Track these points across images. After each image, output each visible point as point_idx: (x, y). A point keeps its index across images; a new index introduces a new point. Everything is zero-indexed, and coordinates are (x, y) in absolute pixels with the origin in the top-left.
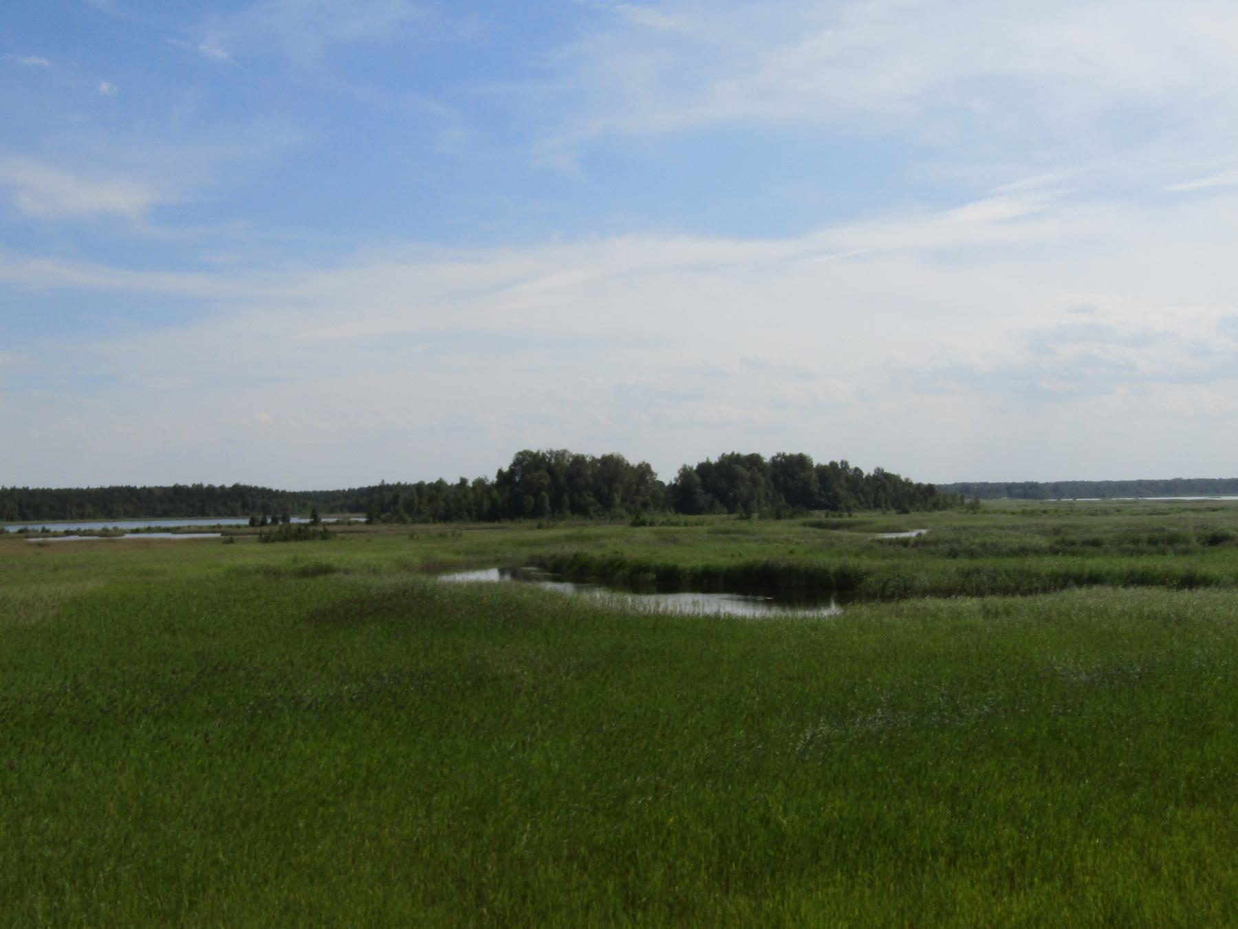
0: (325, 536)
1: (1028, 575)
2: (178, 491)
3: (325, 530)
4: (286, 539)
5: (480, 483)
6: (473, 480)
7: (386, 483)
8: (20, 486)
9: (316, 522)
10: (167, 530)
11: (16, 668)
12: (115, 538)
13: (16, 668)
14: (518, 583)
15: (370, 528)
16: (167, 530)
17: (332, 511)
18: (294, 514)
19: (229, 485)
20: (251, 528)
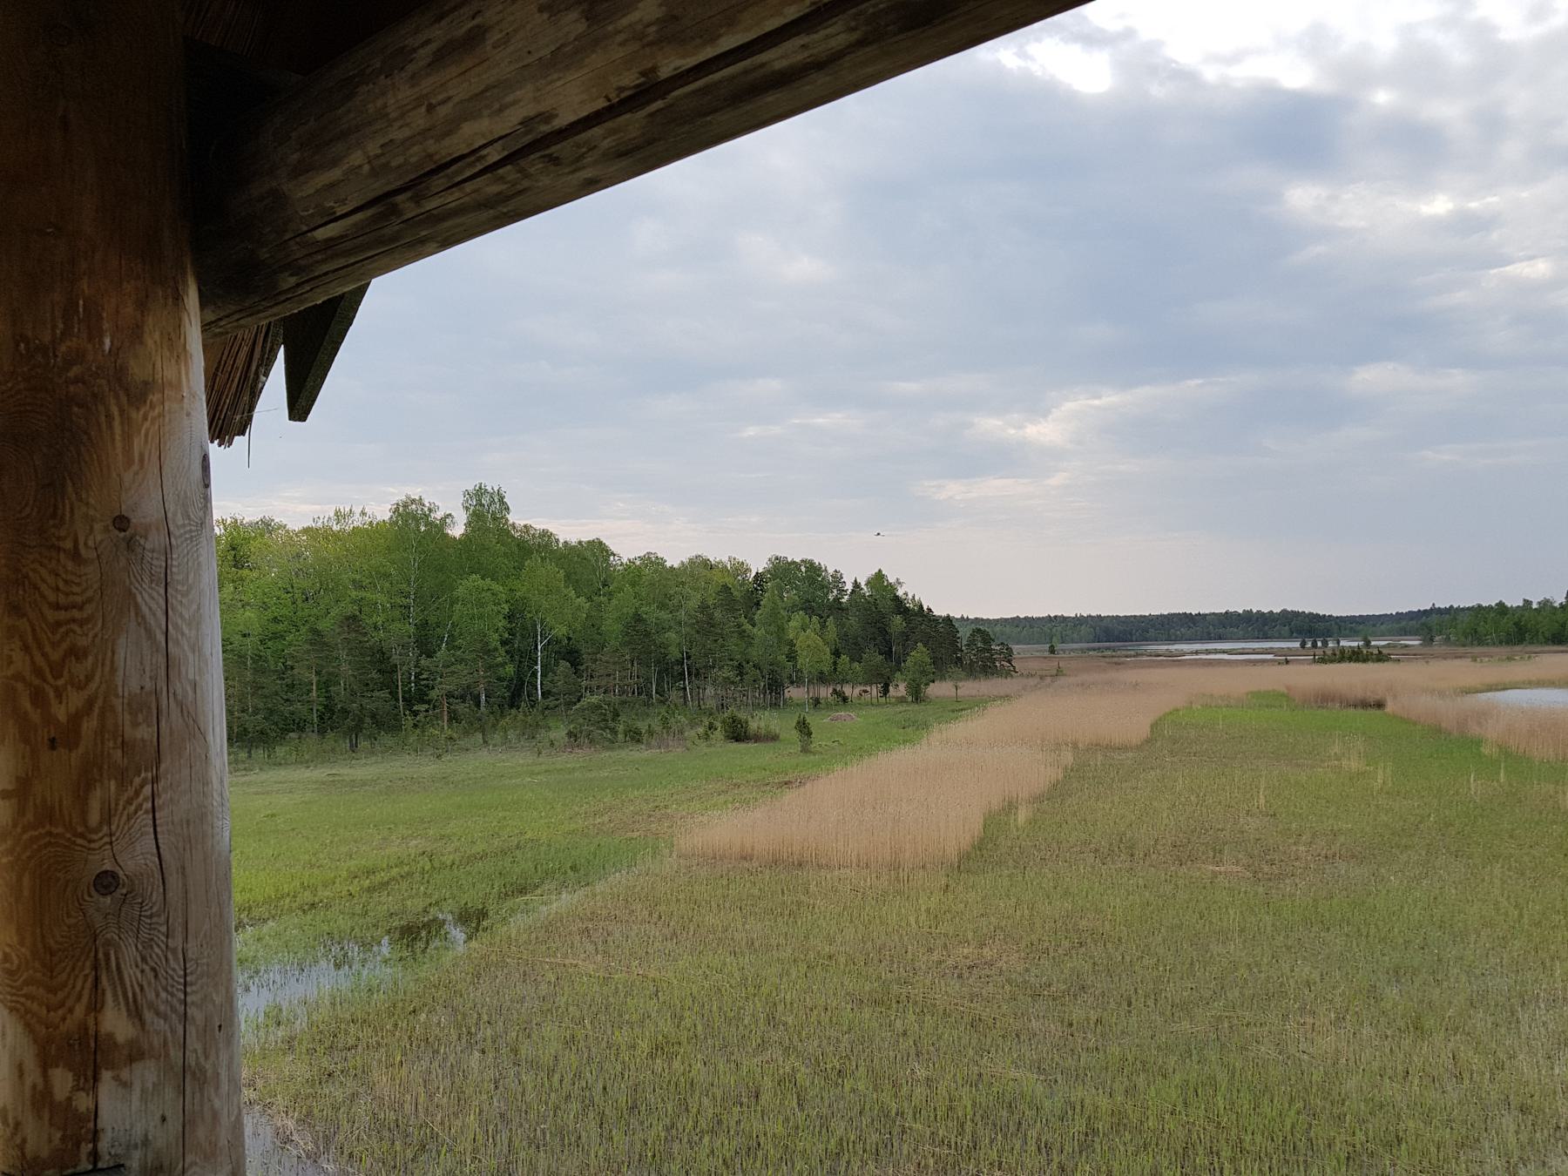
0: (1381, 657)
1: (227, 319)
2: (1228, 616)
3: (1380, 652)
4: (1341, 660)
5: (1545, 604)
6: (865, 579)
7: (1437, 606)
8: (1094, 614)
9: (1368, 644)
10: (1224, 652)
11: (379, 1044)
12: (1180, 658)
13: (379, 1044)
14: (242, 943)
15: (1426, 650)
16: (1224, 652)
17: (1382, 635)
18: (1346, 637)
19: (1277, 610)
20: (1444, 647)
